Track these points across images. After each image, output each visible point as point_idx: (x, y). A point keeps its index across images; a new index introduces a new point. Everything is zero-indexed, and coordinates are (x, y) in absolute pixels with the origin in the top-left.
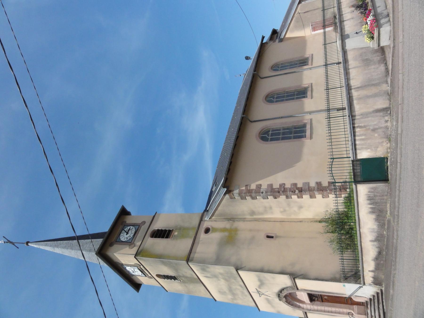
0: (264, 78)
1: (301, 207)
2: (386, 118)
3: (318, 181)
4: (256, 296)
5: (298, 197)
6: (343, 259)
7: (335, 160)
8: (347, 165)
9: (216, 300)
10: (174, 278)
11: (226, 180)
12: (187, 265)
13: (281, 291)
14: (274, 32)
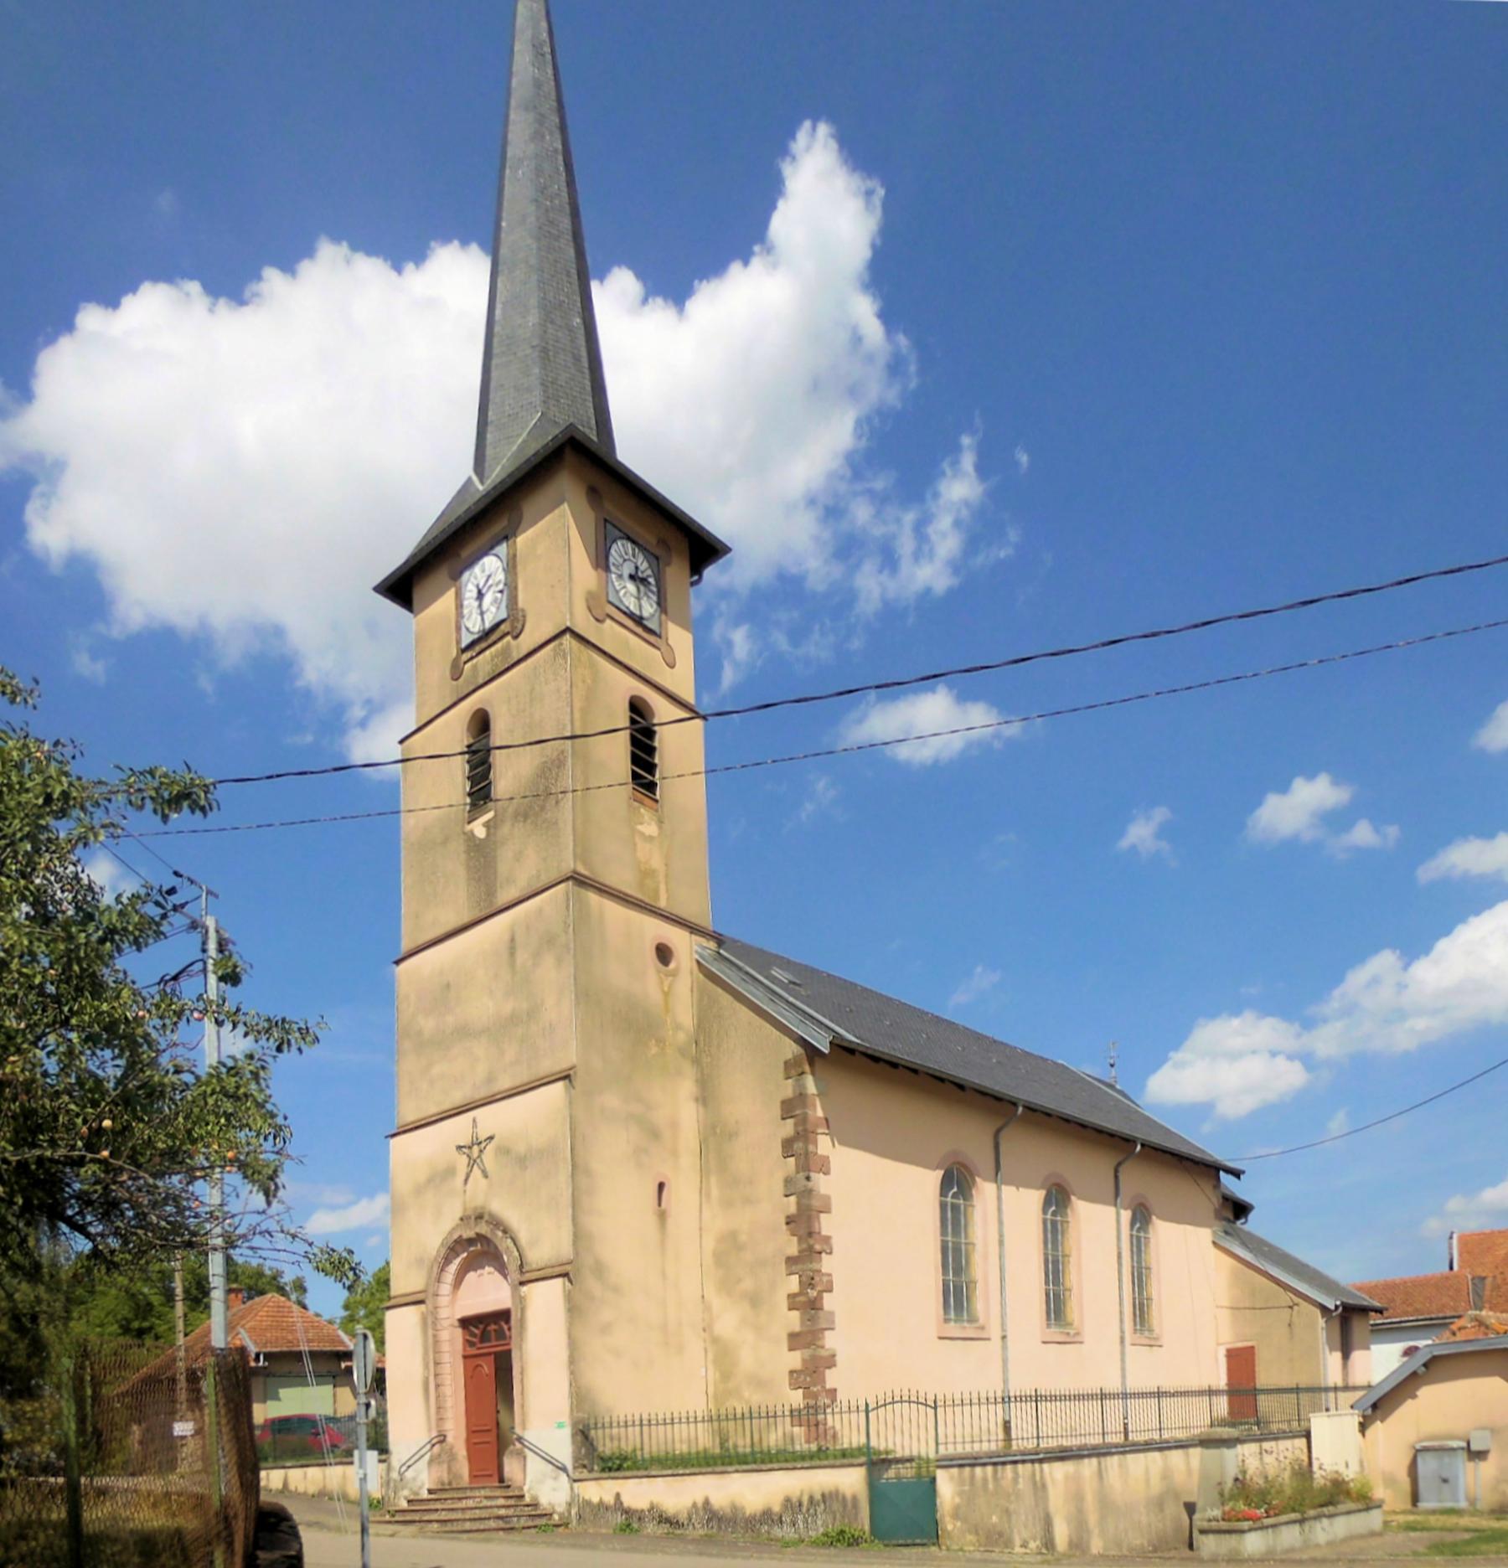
0: (1116, 1177)
1: (755, 1301)
2: (1033, 1545)
3: (838, 1359)
4: (458, 1129)
5: (791, 1296)
6: (641, 1425)
7: (931, 1412)
8: (906, 1444)
9: (397, 962)
10: (480, 792)
11: (850, 1050)
12: (554, 875)
13: (497, 1223)
14: (1240, 1209)
